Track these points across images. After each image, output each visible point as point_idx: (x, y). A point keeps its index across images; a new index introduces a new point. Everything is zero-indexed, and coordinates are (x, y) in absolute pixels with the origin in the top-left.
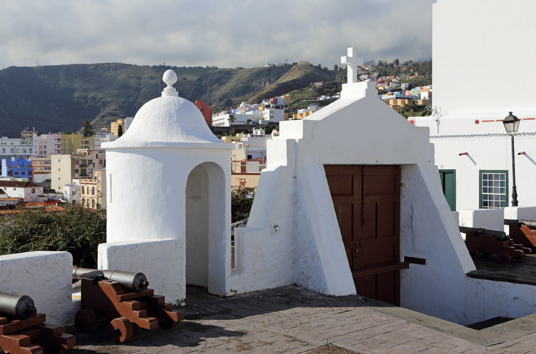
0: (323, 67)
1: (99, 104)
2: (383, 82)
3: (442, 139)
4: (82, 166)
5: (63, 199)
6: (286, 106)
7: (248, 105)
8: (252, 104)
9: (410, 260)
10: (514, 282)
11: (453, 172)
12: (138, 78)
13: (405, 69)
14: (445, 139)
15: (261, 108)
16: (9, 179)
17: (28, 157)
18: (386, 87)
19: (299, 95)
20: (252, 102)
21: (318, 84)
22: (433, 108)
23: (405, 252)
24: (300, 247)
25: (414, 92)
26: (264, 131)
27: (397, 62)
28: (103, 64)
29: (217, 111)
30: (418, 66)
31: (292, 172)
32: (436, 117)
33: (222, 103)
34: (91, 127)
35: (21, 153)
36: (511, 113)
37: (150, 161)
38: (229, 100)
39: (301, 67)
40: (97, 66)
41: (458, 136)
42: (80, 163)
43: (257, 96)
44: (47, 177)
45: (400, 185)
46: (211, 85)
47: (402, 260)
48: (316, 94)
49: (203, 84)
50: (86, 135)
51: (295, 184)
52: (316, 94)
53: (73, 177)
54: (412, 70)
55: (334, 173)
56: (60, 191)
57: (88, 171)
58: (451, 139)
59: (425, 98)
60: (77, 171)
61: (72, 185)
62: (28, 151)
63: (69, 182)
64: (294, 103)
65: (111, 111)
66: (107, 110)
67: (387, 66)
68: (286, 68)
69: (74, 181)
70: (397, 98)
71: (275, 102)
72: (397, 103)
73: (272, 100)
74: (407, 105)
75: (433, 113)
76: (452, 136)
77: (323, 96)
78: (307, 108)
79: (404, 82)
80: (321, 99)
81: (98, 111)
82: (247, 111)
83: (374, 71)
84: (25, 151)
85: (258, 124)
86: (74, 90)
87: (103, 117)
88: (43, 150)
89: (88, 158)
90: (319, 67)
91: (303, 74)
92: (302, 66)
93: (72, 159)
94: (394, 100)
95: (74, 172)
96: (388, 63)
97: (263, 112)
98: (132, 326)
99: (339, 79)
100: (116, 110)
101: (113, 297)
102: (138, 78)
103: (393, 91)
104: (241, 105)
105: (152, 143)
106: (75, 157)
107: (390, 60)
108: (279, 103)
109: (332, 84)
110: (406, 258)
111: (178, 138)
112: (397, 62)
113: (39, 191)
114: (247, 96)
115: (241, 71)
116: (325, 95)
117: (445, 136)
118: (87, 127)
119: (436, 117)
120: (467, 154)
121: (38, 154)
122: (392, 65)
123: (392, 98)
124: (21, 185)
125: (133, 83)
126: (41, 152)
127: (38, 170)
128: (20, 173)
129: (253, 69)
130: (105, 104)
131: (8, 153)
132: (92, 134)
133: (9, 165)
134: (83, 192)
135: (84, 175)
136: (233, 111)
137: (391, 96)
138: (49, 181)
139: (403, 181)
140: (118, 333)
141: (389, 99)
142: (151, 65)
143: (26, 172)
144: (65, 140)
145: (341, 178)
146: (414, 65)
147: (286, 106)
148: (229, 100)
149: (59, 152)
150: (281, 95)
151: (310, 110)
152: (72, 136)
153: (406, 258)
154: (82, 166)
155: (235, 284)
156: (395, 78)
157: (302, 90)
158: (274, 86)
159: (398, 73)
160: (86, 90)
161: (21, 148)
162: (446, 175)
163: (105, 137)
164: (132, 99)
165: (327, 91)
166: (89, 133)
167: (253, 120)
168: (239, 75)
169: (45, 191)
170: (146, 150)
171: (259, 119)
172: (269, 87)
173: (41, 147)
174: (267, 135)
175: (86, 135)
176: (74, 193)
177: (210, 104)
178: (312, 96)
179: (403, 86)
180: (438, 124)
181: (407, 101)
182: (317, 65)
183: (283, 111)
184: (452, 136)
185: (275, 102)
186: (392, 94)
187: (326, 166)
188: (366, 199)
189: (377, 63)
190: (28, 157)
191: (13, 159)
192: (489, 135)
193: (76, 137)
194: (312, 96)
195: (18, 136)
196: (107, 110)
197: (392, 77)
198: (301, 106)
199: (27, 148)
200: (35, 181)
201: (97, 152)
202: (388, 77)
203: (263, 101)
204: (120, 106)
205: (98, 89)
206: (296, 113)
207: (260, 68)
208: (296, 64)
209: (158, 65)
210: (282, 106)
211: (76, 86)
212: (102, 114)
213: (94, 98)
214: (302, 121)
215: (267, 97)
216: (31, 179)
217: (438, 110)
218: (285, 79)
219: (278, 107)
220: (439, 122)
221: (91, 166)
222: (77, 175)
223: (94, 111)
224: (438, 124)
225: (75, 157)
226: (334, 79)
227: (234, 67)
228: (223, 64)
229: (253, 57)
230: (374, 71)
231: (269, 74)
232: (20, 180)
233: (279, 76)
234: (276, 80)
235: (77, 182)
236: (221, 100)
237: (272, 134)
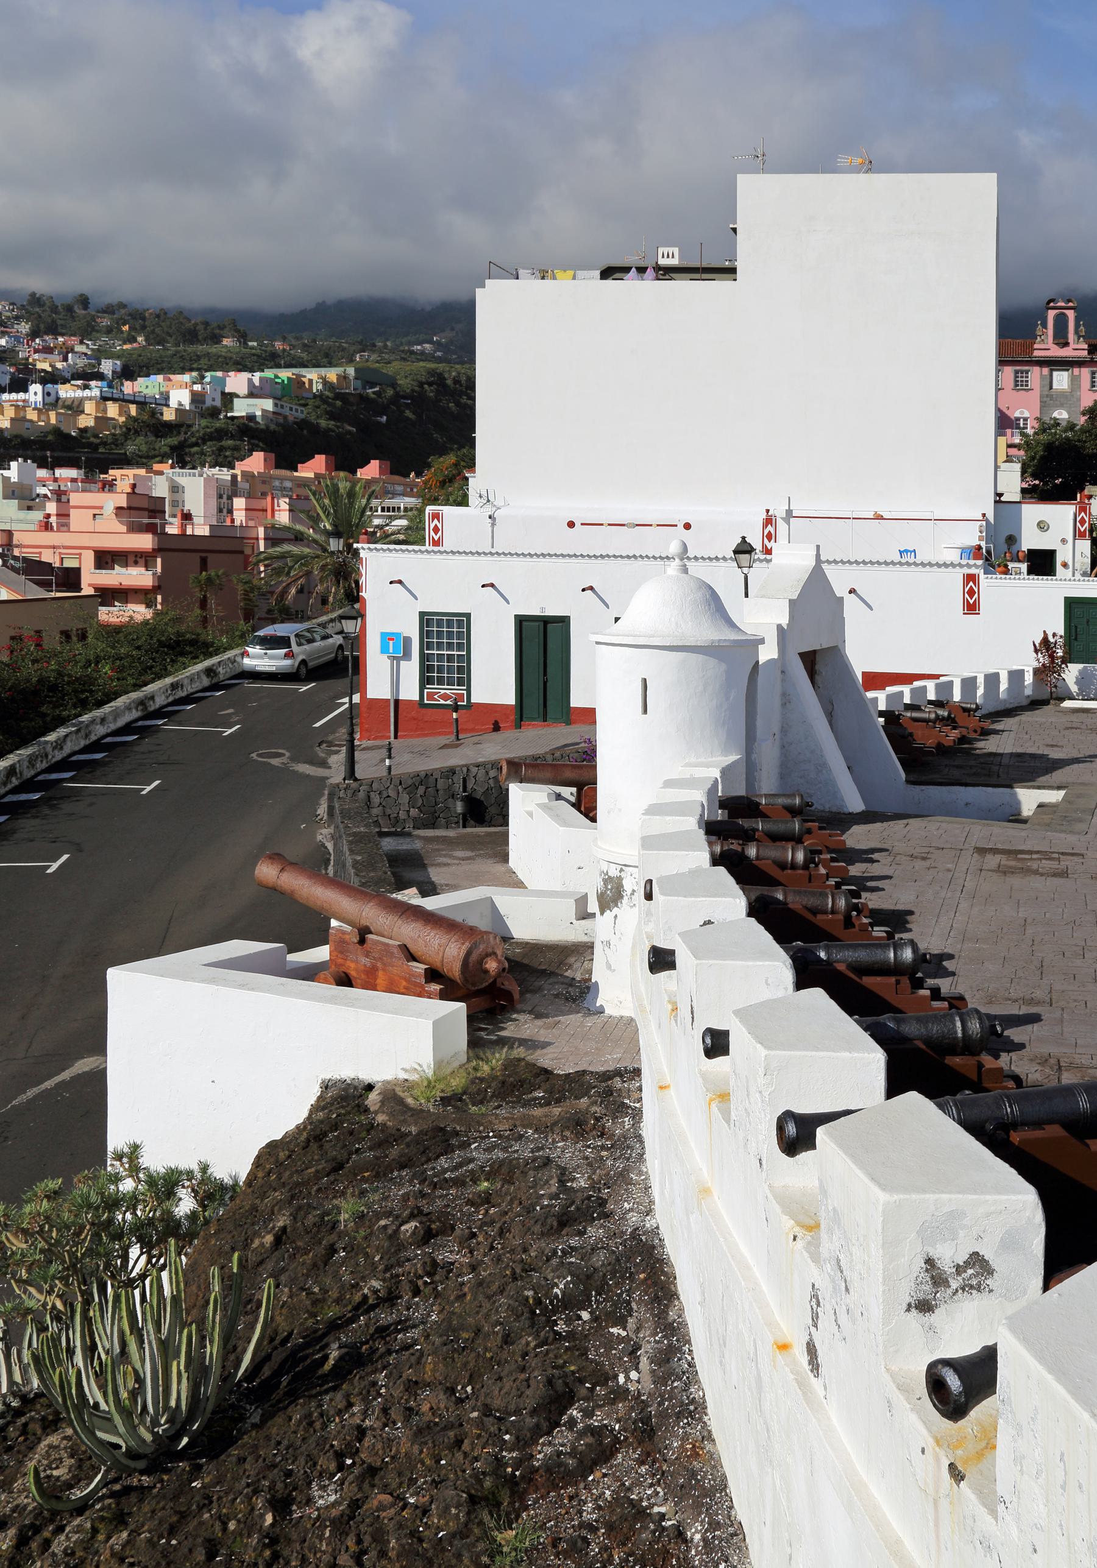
2: (48, 350)
3: (541, 559)
10: (966, 785)
13: (105, 322)
18: (59, 365)
25: (148, 386)
30: (144, 319)
36: (744, 538)
37: (712, 662)
41: (575, 556)
51: (783, 680)
54: (126, 328)
59: (180, 404)
67: (54, 309)
70: (105, 399)
72: (105, 411)
74: (135, 419)
79: (110, 356)
83: (17, 318)
94: (97, 404)
105: (720, 641)
117: (549, 555)
122: (69, 309)
123: (90, 399)
137: (87, 393)
141: (81, 401)
146: (130, 315)
156: (82, 342)
159: (87, 332)
162: (549, 626)
179: (107, 367)
180: (493, 525)
181: (133, 410)
192: (635, 556)
197: (73, 341)
202: (61, 339)
220: (495, 519)
224: (493, 525)
230: (17, 318)
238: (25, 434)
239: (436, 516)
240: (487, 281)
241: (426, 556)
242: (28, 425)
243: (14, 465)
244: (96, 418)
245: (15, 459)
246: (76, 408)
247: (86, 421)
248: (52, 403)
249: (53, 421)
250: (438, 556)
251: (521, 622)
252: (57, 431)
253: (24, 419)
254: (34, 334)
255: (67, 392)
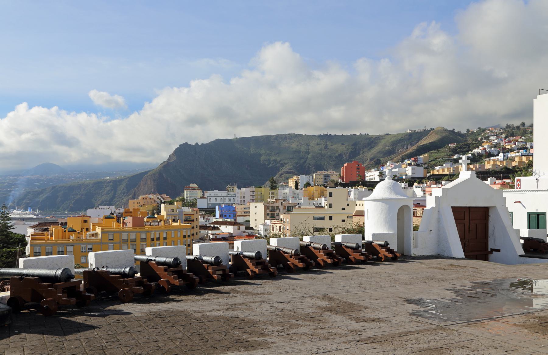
0: (456, 131)
1: (278, 165)
2: (510, 142)
4: (271, 211)
5: (258, 234)
6: (425, 164)
7: (394, 163)
8: (397, 162)
9: (493, 250)
11: (544, 214)
12: (307, 145)
14: (539, 192)
15: (404, 166)
16: (221, 220)
17: (233, 204)
18: (513, 146)
19: (436, 154)
20: (397, 161)
21: (452, 146)
22: (534, 171)
23: (491, 246)
24: (441, 239)
26: (407, 184)
27: (523, 124)
28: (281, 135)
29: (369, 169)
31: (438, 209)
32: (536, 177)
33: (373, 162)
34: (275, 182)
35: (227, 202)
37: (384, 204)
38: (378, 160)
39: (437, 132)
40: (277, 137)
42: (270, 208)
43: (401, 156)
44: (247, 218)
45: (489, 216)
46: (363, 149)
47: (490, 250)
48: (450, 153)
49: (357, 148)
50: (272, 188)
52: (450, 153)
53: (265, 219)
55: (455, 209)
56: (257, 228)
57: (275, 215)
58: (543, 192)
60: (268, 214)
61: (265, 225)
62: (232, 200)
63: (263, 222)
64: (431, 161)
65: (288, 170)
66: (285, 169)
67: (514, 128)
68: (425, 133)
69: (266, 221)
70: (522, 155)
71: (416, 160)
72: (522, 159)
73: (413, 159)
75: (534, 174)
76: (533, 191)
77: (457, 155)
78: (442, 165)
80: (455, 157)
81: (278, 170)
82: (393, 169)
83: (502, 133)
84: (230, 200)
85: (402, 179)
86: (260, 155)
87: (282, 174)
88: (243, 200)
89: (276, 205)
90: (453, 131)
91: (440, 137)
92: (438, 131)
93: (265, 206)
94: (519, 157)
95: (266, 215)
96: (515, 126)
97: (407, 169)
98: (386, 256)
99: (471, 140)
100: (291, 169)
101: (378, 248)
102: (307, 145)
103: (519, 149)
104: (388, 164)
106: (267, 204)
107: (516, 123)
108: (419, 162)
109: (465, 145)
110: (491, 249)
111: (394, 196)
112: (523, 124)
113: (243, 228)
114: (393, 156)
115: (388, 136)
116: (458, 154)
118: (272, 183)
119: (536, 177)
120: (520, 202)
121: (239, 202)
122: (518, 127)
124: (230, 224)
125: (303, 149)
126: (241, 201)
127: (239, 213)
128: (228, 215)
129: (397, 134)
130: (283, 165)
131: (219, 201)
132: (276, 187)
133: (220, 209)
134: (273, 230)
135: (273, 217)
136: (381, 169)
137: (517, 154)
138: (249, 221)
139: (490, 214)
140: (381, 258)
142: (317, 134)
143: (232, 215)
144: (257, 192)
145: (462, 214)
147: (425, 164)
148: (378, 160)
149: (253, 201)
150: (421, 155)
151: (445, 167)
152: (263, 189)
153: (491, 249)
154: (271, 211)
155: (414, 252)
157: (438, 151)
158: (414, 148)
160: (269, 155)
161: (227, 198)
163: (286, 189)
164: (302, 161)
165: (460, 151)
166: (274, 186)
167: (398, 175)
168: (386, 139)
169: (247, 229)
170: (382, 201)
171: (403, 174)
172: (411, 149)
173: (241, 197)
174: (409, 188)
175: (272, 188)
176: (266, 230)
177: (363, 163)
178: (447, 155)
180: (538, 182)
182: (452, 130)
183: (422, 168)
184: (533, 191)
185: (416, 160)
186: (518, 152)
187: (452, 207)
188: (471, 221)
189: (504, 126)
190: (233, 204)
191: (223, 206)
193: (265, 190)
194: (447, 155)
195: (225, 190)
196: (285, 169)
198: (438, 163)
199: (232, 198)
200: (238, 221)
201: (282, 201)
203: (406, 160)
204: (294, 166)
205: (278, 153)
206: (434, 169)
207: (403, 134)
208: (434, 129)
209: (322, 134)
210: (422, 164)
211: (262, 152)
212: (280, 172)
213: (275, 161)
214: (441, 189)
215: (409, 156)
216: (235, 220)
217: (538, 172)
218: (424, 142)
219: (418, 165)
221: (278, 211)
222: (268, 217)
223: (275, 170)
224: (538, 182)
225: (267, 204)
226: (466, 141)
227: (381, 133)
228: (372, 132)
229: (397, 126)
230: (502, 133)
231: (410, 139)
232: (229, 220)
233: (419, 139)
234: (417, 142)
235: (268, 222)
236: (371, 159)
237: (414, 186)
238: (496, 169)
239: (518, 180)
240: (538, 96)
241: (515, 193)
242: (497, 166)
243: (489, 179)
244: (519, 162)
245: (489, 177)
246: (513, 159)
247: (515, 164)
248: (506, 159)
249: (505, 164)
250: (519, 193)
251: (529, 214)
252: (506, 168)
253: (496, 165)
254: (506, 137)
255: (511, 155)
